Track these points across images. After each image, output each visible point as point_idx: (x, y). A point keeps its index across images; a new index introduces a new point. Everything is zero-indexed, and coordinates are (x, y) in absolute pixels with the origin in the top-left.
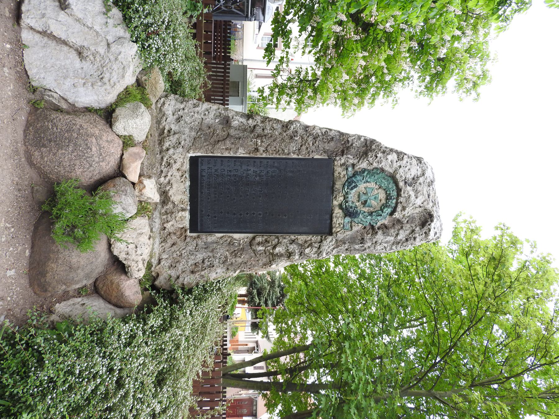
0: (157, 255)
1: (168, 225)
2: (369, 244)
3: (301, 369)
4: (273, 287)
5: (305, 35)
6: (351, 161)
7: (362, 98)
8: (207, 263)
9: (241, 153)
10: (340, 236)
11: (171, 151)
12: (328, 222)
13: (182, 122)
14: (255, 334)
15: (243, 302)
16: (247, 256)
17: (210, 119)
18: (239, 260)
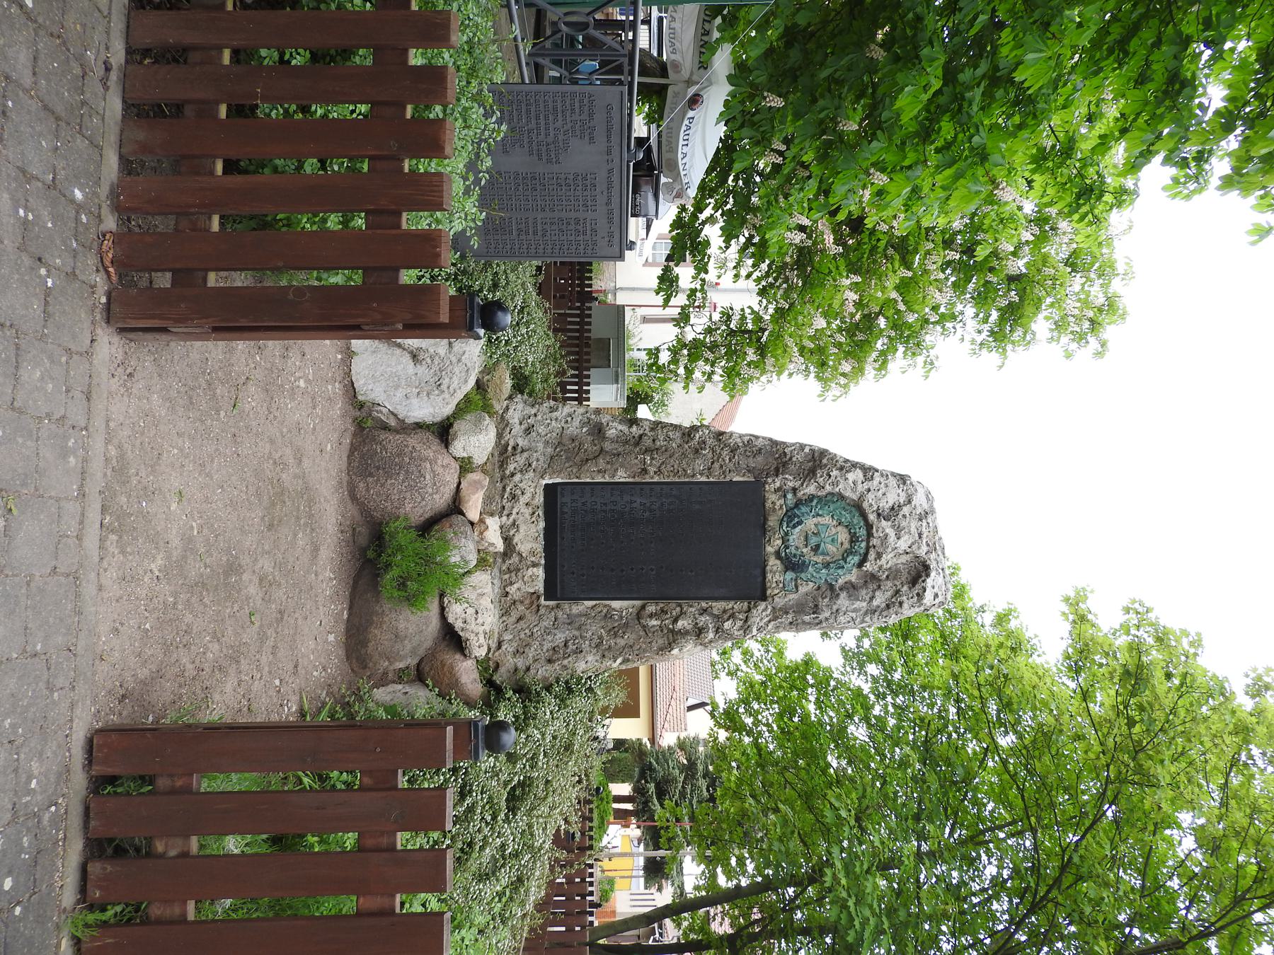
0: (496, 635)
1: (512, 590)
2: (827, 614)
3: (754, 937)
4: (693, 776)
5: (734, 247)
6: (791, 484)
7: (859, 361)
8: (571, 647)
9: (621, 476)
10: (779, 602)
11: (517, 477)
12: (760, 579)
13: (534, 434)
14: (653, 890)
15: (622, 816)
16: (634, 636)
17: (574, 428)
18: (621, 642)
